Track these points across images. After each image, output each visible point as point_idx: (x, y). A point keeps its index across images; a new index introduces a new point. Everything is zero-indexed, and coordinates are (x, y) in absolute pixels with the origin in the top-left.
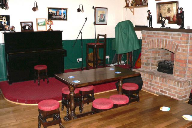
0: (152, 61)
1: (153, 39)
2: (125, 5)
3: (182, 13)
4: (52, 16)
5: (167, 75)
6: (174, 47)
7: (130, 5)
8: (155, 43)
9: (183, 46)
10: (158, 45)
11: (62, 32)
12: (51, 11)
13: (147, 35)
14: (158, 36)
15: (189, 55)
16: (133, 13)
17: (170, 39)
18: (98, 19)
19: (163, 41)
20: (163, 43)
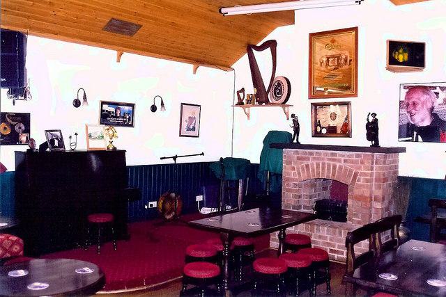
0: (305, 201)
1: (309, 163)
2: (236, 101)
3: (375, 122)
4: (108, 119)
5: (337, 224)
6: (350, 175)
7: (244, 101)
8: (313, 170)
9: (365, 174)
10: (318, 174)
11: (126, 153)
12: (106, 107)
13: (296, 156)
14: (318, 159)
15: (376, 188)
16: (248, 117)
17: (342, 164)
18: (185, 125)
19: (329, 165)
20: (329, 169)
